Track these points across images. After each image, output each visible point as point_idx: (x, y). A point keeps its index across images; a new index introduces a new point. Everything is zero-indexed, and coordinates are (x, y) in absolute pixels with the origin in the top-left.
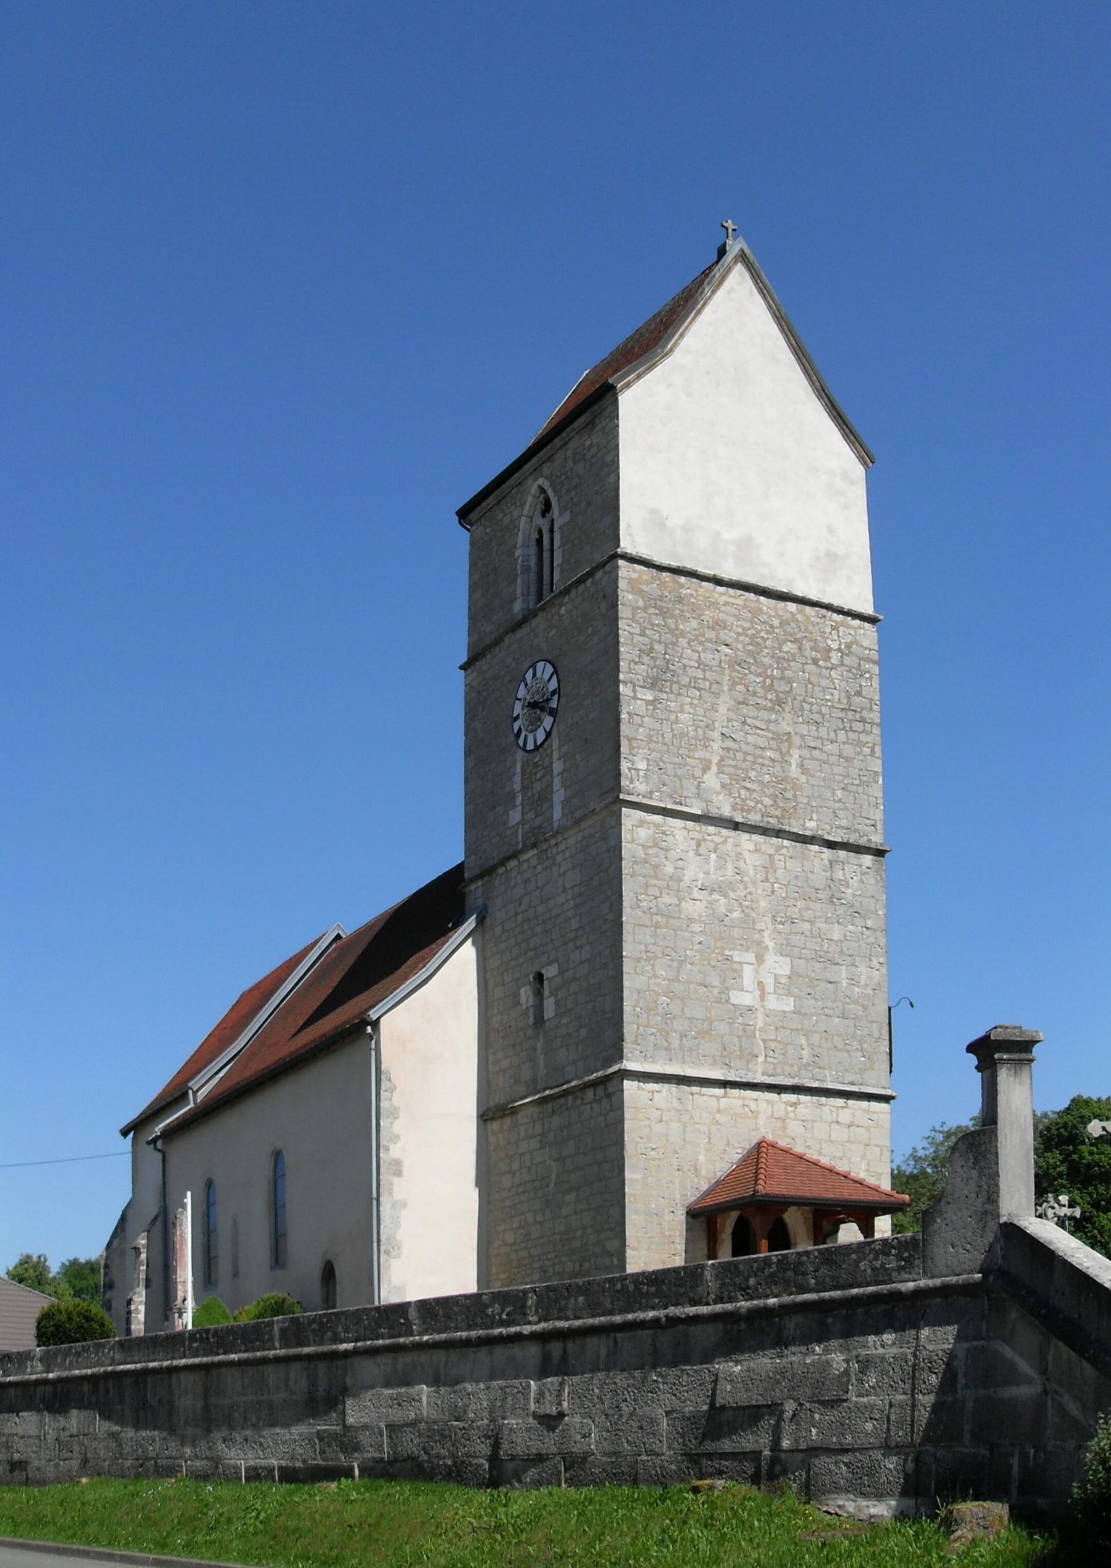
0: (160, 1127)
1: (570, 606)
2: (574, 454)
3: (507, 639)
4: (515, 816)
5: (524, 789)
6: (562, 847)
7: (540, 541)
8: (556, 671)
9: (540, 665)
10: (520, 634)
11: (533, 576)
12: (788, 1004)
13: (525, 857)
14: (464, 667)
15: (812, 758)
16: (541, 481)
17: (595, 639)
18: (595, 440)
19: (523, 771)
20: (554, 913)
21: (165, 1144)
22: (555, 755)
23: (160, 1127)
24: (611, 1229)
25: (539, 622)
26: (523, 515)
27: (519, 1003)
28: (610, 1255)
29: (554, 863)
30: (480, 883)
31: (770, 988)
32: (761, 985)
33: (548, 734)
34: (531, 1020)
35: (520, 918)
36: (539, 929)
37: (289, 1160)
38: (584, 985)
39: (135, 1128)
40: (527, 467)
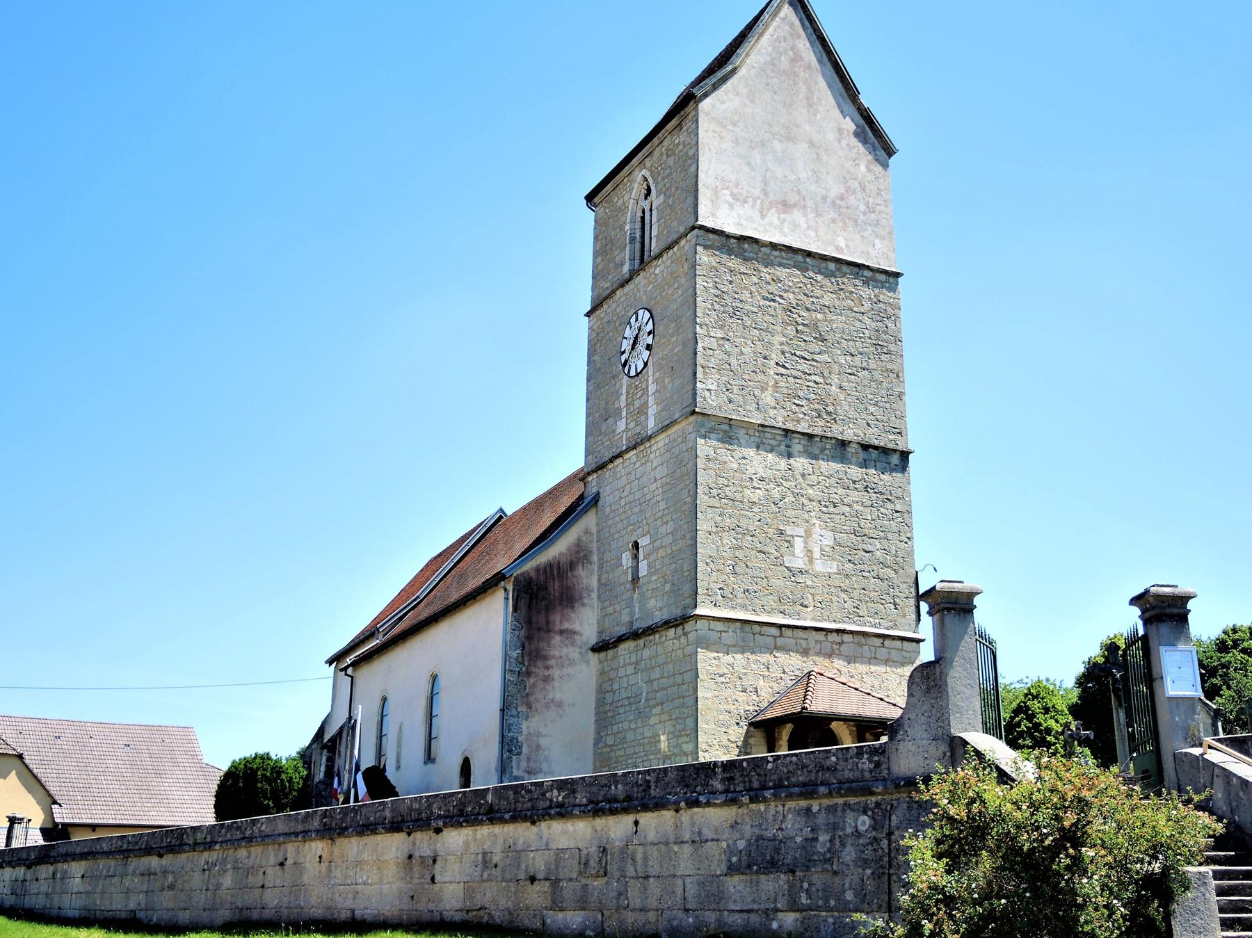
0: (348, 661)
1: (662, 267)
2: (667, 150)
3: (618, 292)
4: (621, 426)
5: (628, 405)
6: (654, 448)
7: (643, 218)
8: (652, 316)
9: (640, 313)
10: (627, 289)
11: (638, 245)
12: (832, 567)
13: (627, 456)
14: (588, 315)
15: (849, 381)
16: (644, 172)
17: (680, 292)
18: (682, 138)
19: (628, 392)
20: (648, 497)
21: (354, 671)
22: (650, 381)
23: (348, 661)
24: (687, 735)
25: (640, 279)
26: (630, 196)
27: (621, 565)
28: (686, 754)
29: (648, 461)
30: (595, 475)
31: (817, 554)
32: (809, 552)
33: (646, 364)
34: (630, 578)
35: (623, 502)
36: (636, 510)
37: (442, 683)
38: (669, 551)
39: (336, 659)
40: (635, 161)
